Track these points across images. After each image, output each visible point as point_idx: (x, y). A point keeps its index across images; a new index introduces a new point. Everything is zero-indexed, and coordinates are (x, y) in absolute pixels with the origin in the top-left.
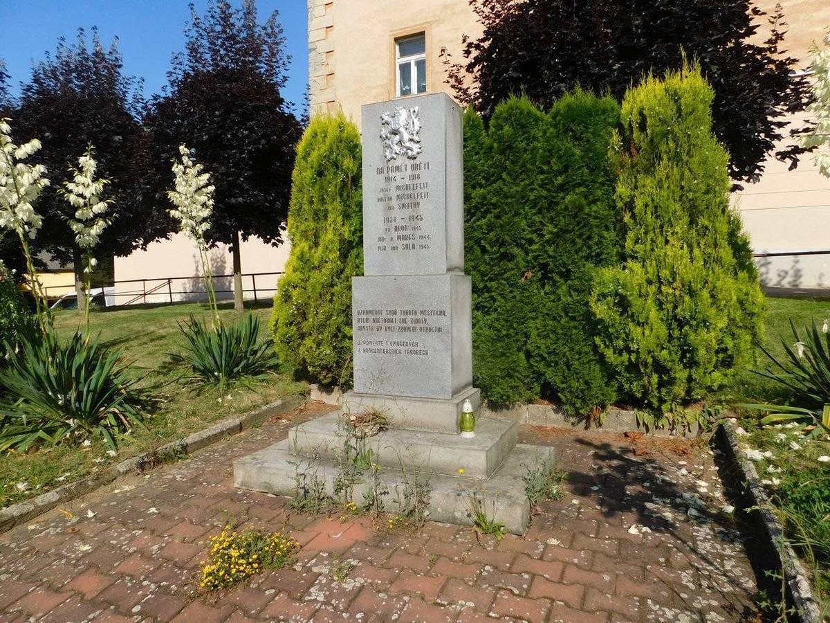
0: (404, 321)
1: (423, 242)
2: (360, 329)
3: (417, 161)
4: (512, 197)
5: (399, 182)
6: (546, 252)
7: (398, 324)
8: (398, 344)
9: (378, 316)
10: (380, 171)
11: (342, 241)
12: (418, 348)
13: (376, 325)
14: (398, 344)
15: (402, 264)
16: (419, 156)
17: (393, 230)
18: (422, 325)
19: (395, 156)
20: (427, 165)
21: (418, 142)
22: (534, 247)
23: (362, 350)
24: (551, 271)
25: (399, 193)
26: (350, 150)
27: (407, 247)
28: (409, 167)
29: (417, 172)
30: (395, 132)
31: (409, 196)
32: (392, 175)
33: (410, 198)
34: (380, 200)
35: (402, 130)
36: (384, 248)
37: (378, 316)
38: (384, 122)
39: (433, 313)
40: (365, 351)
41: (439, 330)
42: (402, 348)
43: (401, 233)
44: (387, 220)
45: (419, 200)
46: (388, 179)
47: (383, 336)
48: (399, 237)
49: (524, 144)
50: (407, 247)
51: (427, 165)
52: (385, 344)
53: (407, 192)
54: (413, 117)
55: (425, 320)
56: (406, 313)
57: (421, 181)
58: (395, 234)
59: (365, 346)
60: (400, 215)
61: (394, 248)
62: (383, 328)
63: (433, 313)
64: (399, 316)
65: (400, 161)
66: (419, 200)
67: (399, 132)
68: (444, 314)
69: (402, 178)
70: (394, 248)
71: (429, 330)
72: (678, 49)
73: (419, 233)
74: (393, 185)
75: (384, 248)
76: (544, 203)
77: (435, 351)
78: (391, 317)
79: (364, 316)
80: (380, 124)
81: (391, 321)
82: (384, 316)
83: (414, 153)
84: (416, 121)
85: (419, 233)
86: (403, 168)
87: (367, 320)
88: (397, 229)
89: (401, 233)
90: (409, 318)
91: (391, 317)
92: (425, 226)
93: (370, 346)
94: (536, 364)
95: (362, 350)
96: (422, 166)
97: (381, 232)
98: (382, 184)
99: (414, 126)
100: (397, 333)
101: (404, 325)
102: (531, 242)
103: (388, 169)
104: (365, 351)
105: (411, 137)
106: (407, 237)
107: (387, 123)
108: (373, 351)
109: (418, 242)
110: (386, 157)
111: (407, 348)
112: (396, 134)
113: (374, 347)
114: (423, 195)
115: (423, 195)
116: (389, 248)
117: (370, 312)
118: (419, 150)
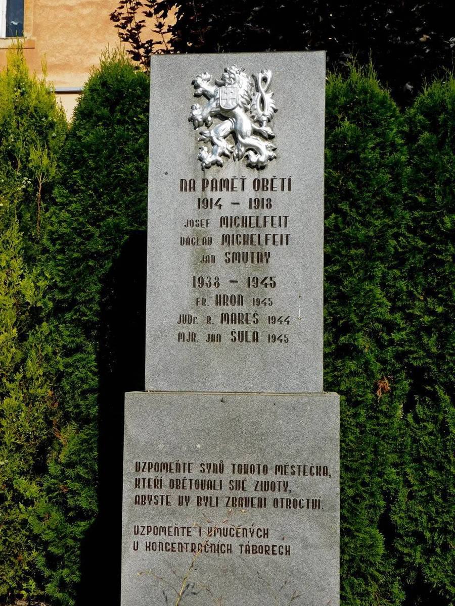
0: (240, 485)
1: (276, 329)
2: (140, 500)
3: (267, 174)
4: (357, 246)
5: (227, 211)
6: (422, 346)
7: (226, 492)
8: (224, 532)
9: (182, 475)
10: (186, 186)
11: (21, 306)
12: (269, 541)
13: (175, 494)
14: (224, 532)
15: (228, 370)
16: (270, 165)
17: (211, 302)
18: (278, 495)
19: (221, 159)
20: (286, 184)
21: (270, 138)
22: (396, 336)
23: (142, 547)
24: (432, 382)
25: (227, 231)
26: (40, 133)
27: (242, 336)
28: (249, 184)
29: (267, 195)
30: (223, 115)
31: (248, 240)
32: (215, 195)
33: (250, 242)
34: (185, 241)
35: (239, 111)
36: (193, 337)
37: (182, 475)
38: (199, 91)
39: (303, 470)
40: (149, 547)
41: (316, 504)
42: (234, 542)
43: (229, 309)
44: (199, 282)
45: (270, 247)
46: (205, 203)
47: (192, 516)
48: (224, 318)
49: (376, 154)
50: (242, 336)
51: (286, 184)
52: (195, 533)
53: (243, 231)
54: (263, 89)
55: (286, 485)
56: (243, 469)
57: (277, 210)
58: (216, 312)
59: (151, 538)
60: (228, 275)
61: (212, 338)
62: (194, 500)
63: (303, 470)
64: (228, 475)
65: (231, 171)
66: (270, 247)
67: (234, 116)
68: (326, 473)
69: (235, 202)
70: (212, 338)
71: (296, 504)
72: (331, 27)
73: (268, 311)
74: (215, 215)
75: (193, 337)
76: (416, 260)
77: (305, 547)
78: (212, 476)
79: (152, 475)
80: (190, 95)
81: (211, 485)
82: (196, 474)
83: (262, 159)
84: (268, 98)
85: (268, 311)
86: (238, 184)
87: (158, 483)
88: (219, 300)
89: (229, 309)
90: (251, 479)
91: (212, 476)
92: (281, 299)
93: (162, 538)
94: (406, 551)
95: (142, 547)
96: (277, 183)
97: (186, 304)
98: (190, 210)
99: (263, 108)
100: (222, 509)
101: (240, 494)
102: (390, 327)
103: (203, 184)
104: (149, 547)
105: (257, 127)
106: (242, 319)
107: (206, 95)
108: (164, 547)
109: (265, 329)
110: (201, 159)
111: (244, 541)
112: (223, 118)
113: (170, 540)
114: (278, 239)
115: (278, 239)
116: (202, 337)
117: (165, 467)
118: (272, 154)
